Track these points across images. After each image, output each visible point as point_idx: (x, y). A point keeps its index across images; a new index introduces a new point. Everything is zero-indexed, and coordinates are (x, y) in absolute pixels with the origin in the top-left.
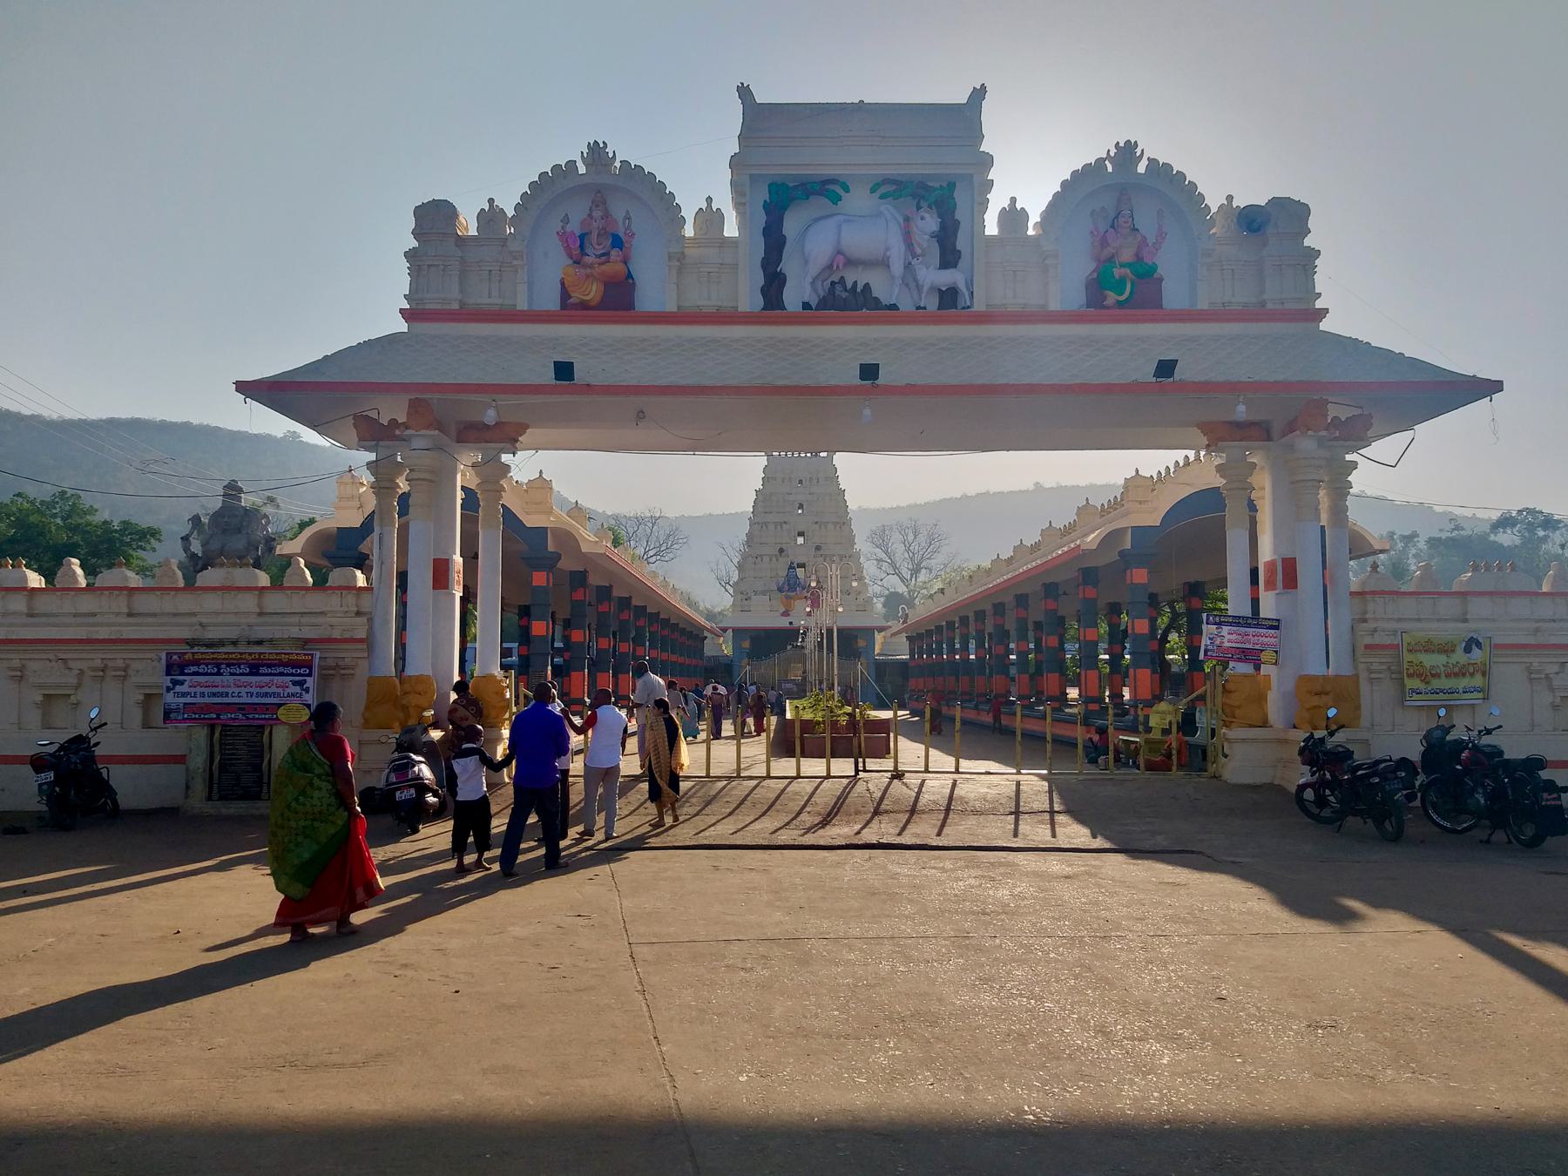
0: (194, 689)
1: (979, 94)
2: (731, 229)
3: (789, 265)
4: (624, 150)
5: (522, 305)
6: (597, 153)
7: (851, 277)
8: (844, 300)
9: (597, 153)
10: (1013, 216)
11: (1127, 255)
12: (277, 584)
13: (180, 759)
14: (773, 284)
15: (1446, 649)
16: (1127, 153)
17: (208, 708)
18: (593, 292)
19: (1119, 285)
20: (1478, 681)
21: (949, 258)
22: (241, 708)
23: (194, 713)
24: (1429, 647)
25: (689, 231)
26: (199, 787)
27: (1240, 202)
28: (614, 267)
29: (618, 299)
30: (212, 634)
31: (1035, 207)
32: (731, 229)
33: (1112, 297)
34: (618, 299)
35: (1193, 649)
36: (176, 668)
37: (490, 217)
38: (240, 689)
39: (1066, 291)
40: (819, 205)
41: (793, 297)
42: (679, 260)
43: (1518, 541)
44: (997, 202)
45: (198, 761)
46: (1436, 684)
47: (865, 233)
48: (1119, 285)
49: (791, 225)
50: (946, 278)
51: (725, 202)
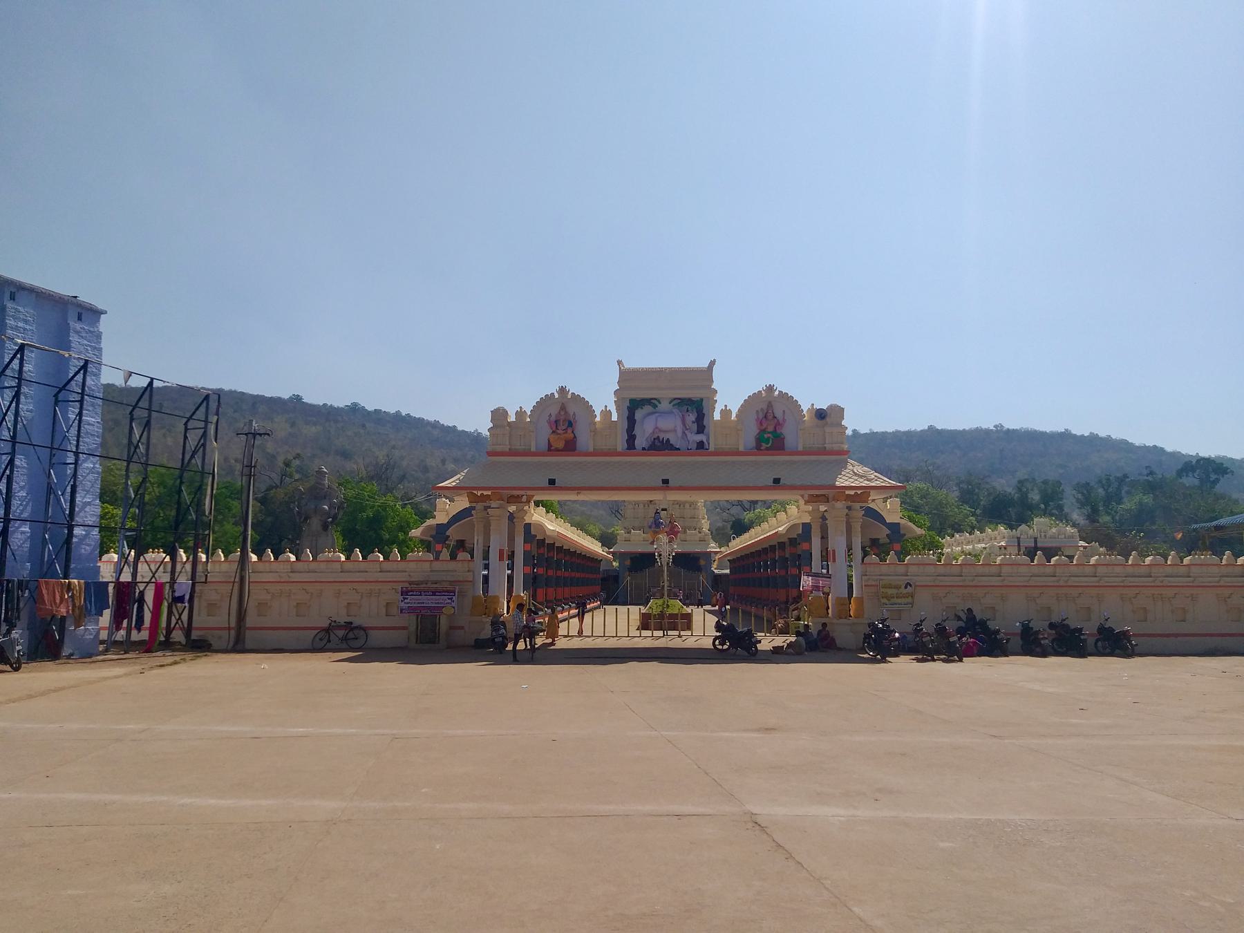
0: (412, 601)
1: (713, 363)
2: (615, 417)
3: (637, 431)
4: (573, 389)
5: (533, 449)
6: (562, 390)
7: (662, 436)
8: (660, 446)
9: (562, 390)
10: (726, 413)
11: (771, 429)
12: (437, 559)
13: (404, 628)
14: (631, 439)
15: (898, 587)
16: (770, 389)
17: (416, 608)
18: (561, 445)
19: (767, 441)
20: (910, 600)
21: (701, 429)
22: (429, 608)
23: (411, 610)
24: (890, 587)
25: (598, 419)
26: (413, 639)
27: (817, 406)
28: (569, 435)
29: (570, 447)
30: (418, 583)
31: (735, 409)
32: (615, 417)
33: (764, 446)
34: (570, 447)
35: (134, 574)
36: (405, 593)
37: (520, 414)
38: (430, 601)
39: (747, 439)
40: (648, 409)
41: (640, 442)
42: (595, 432)
43: (1197, 482)
44: (719, 407)
45: (413, 628)
46: (893, 601)
47: (671, 425)
48: (767, 441)
49: (639, 414)
50: (700, 437)
51: (612, 408)
